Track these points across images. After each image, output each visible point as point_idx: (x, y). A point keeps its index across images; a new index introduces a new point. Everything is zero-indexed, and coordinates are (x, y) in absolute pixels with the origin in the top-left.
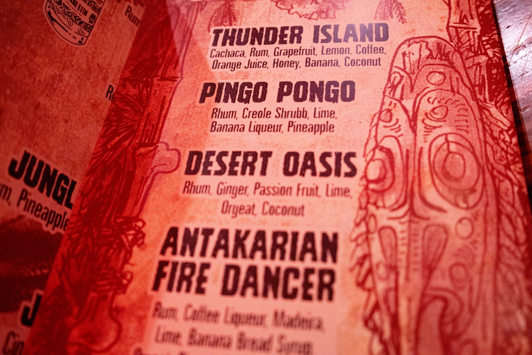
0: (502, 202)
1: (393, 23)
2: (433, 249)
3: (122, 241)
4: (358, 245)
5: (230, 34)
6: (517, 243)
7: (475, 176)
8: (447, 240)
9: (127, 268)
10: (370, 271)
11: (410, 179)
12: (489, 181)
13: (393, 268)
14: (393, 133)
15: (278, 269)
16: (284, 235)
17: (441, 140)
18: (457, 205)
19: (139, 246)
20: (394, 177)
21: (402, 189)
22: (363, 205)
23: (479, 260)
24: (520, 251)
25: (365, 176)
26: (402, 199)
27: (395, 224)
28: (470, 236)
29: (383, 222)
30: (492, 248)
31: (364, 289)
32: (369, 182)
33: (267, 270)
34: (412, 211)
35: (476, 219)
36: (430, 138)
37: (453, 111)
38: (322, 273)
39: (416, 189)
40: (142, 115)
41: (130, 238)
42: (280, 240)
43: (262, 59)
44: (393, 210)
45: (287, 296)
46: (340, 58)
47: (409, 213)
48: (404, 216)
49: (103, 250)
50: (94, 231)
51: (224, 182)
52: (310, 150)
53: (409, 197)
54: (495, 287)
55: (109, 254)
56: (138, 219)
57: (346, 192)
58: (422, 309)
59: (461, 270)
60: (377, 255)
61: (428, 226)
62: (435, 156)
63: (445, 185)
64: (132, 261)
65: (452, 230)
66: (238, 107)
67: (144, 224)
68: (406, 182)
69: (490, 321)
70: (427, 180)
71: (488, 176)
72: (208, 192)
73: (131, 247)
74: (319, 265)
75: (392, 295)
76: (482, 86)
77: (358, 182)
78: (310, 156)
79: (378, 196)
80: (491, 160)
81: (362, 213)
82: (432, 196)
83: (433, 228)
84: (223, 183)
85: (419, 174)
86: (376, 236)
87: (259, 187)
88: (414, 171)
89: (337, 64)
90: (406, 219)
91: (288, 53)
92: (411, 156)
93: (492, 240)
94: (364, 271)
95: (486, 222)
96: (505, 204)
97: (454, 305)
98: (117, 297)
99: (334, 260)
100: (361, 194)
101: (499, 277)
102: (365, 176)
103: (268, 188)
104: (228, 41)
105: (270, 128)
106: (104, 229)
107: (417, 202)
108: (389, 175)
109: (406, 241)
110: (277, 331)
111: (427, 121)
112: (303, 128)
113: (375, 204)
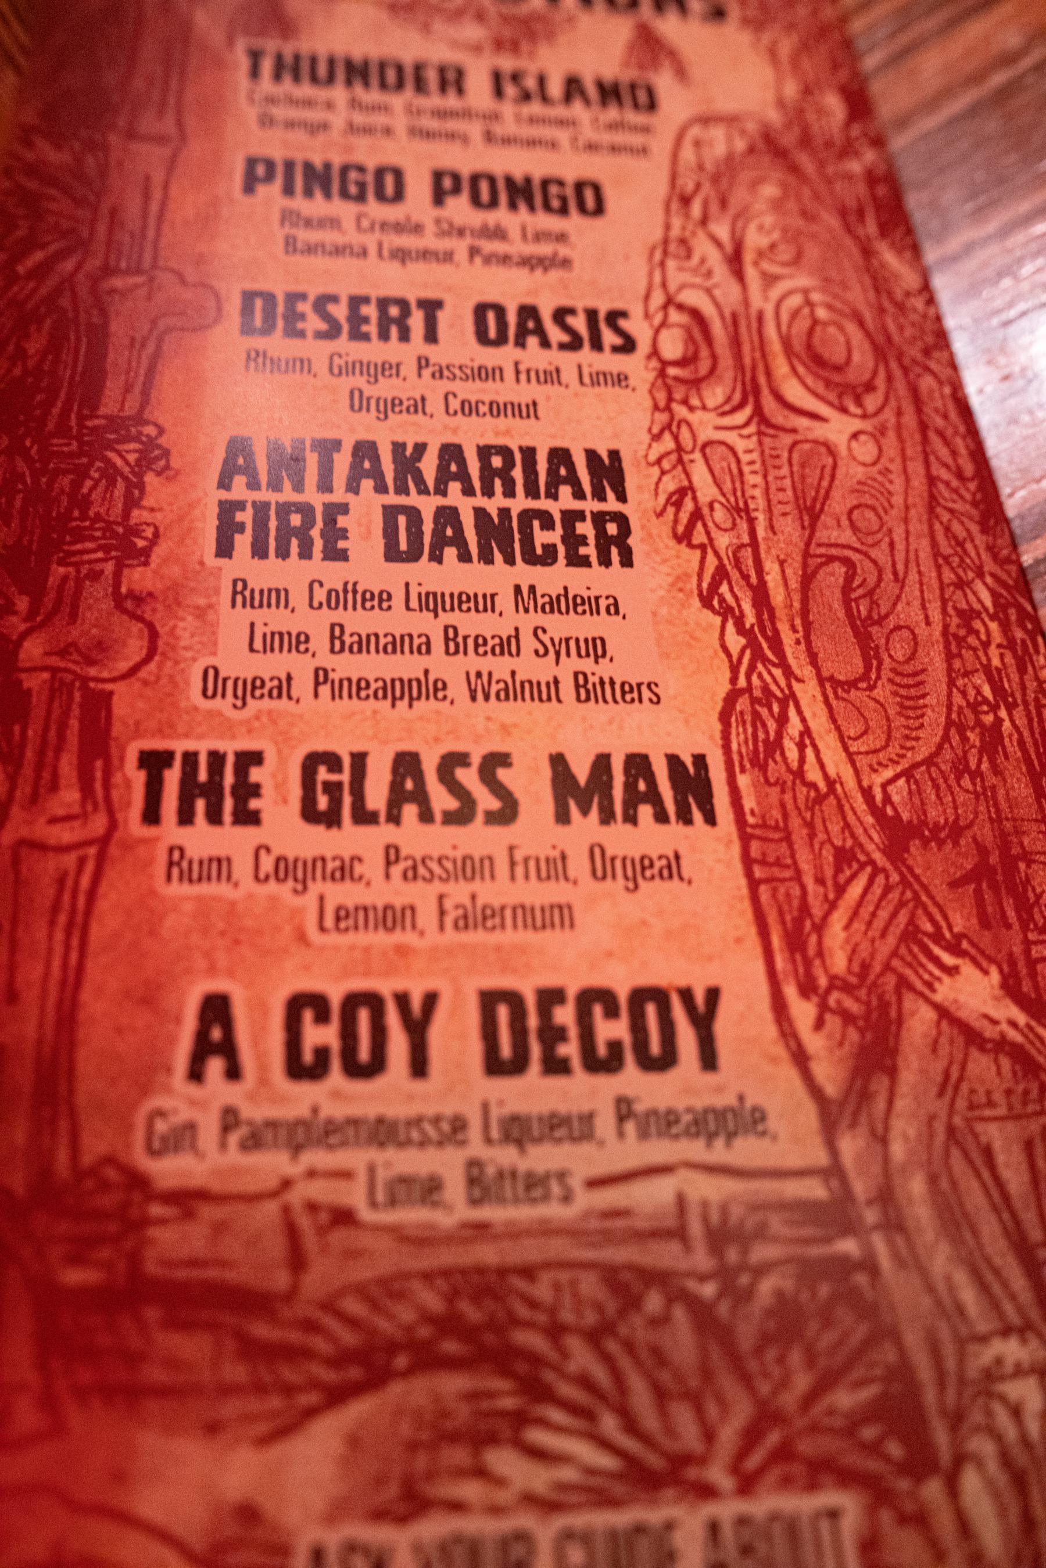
0: (939, 510)
1: (664, 82)
2: (812, 479)
3: (108, 461)
4: (663, 472)
5: (203, 776)
6: (960, 475)
7: (871, 364)
8: (835, 467)
9: (137, 516)
10: (697, 515)
11: (747, 361)
12: (898, 373)
13: (741, 511)
14: (698, 280)
15: (504, 513)
16: (505, 452)
17: (796, 300)
18: (844, 410)
19: (159, 474)
20: (714, 357)
21: (735, 381)
22: (662, 404)
23: (898, 500)
24: (967, 489)
25: (655, 352)
26: (737, 397)
27: (731, 437)
28: (874, 464)
29: (706, 434)
30: (919, 482)
31: (690, 545)
32: (665, 363)
33: (480, 514)
34: (758, 412)
35: (883, 434)
36: (775, 293)
37: (813, 252)
38: (600, 519)
39: (762, 380)
40: (95, 209)
41: (132, 458)
42: (497, 462)
43: (379, 120)
44: (724, 414)
45: (531, 558)
46: (563, 136)
47: (755, 420)
48: (747, 424)
49: (65, 481)
50: (28, 443)
51: (343, 352)
52: (529, 300)
53: (750, 393)
54: (934, 544)
55: (85, 490)
56: (139, 420)
57: (621, 380)
58: (807, 580)
59: (870, 515)
60: (706, 489)
61: (795, 443)
62: (790, 326)
63: (817, 375)
64: (148, 502)
65: (843, 451)
66: (344, 210)
67: (161, 431)
68: (739, 366)
69: (933, 596)
70: (781, 367)
71: (894, 365)
72: (309, 371)
73: (140, 476)
74: (590, 505)
75: (747, 554)
76: (861, 213)
77: (643, 362)
78: (528, 312)
79: (689, 389)
80: (896, 338)
81: (662, 418)
82: (795, 392)
83: (807, 446)
84: (340, 356)
85: (764, 356)
86: (697, 455)
87: (397, 859)
88: (753, 349)
89: (553, 145)
90: (752, 429)
91: (441, 114)
92: (743, 324)
93: (917, 468)
94: (684, 517)
95: (901, 439)
96: (933, 414)
97: (866, 571)
98: (126, 571)
99: (622, 497)
100: (653, 385)
101: (937, 526)
102: (655, 352)
103: (423, 860)
104: (200, 805)
105: (425, 255)
106: (55, 441)
107: (769, 403)
108: (704, 353)
109: (757, 467)
110: (527, 622)
111: (766, 265)
112: (505, 260)
113: (685, 402)
